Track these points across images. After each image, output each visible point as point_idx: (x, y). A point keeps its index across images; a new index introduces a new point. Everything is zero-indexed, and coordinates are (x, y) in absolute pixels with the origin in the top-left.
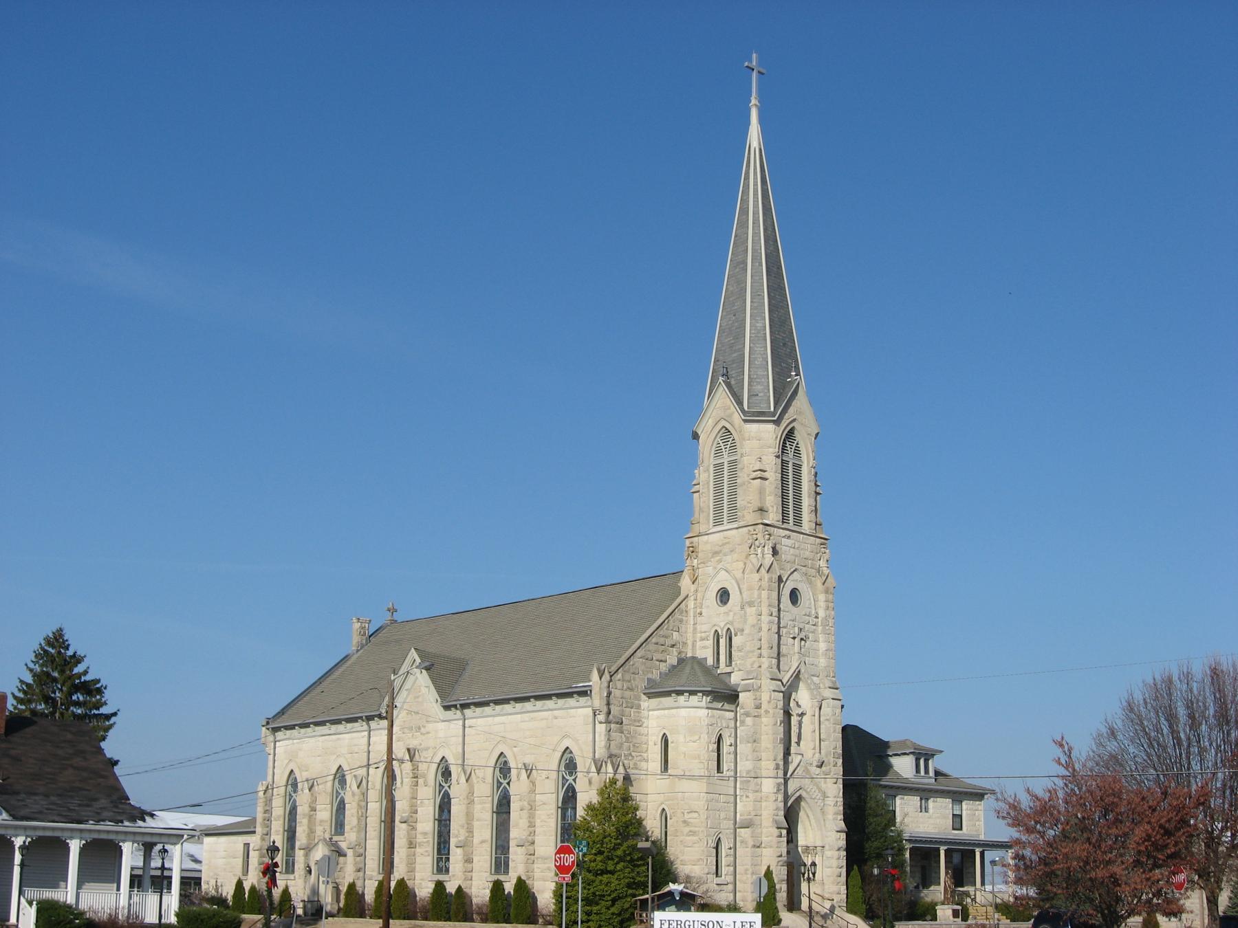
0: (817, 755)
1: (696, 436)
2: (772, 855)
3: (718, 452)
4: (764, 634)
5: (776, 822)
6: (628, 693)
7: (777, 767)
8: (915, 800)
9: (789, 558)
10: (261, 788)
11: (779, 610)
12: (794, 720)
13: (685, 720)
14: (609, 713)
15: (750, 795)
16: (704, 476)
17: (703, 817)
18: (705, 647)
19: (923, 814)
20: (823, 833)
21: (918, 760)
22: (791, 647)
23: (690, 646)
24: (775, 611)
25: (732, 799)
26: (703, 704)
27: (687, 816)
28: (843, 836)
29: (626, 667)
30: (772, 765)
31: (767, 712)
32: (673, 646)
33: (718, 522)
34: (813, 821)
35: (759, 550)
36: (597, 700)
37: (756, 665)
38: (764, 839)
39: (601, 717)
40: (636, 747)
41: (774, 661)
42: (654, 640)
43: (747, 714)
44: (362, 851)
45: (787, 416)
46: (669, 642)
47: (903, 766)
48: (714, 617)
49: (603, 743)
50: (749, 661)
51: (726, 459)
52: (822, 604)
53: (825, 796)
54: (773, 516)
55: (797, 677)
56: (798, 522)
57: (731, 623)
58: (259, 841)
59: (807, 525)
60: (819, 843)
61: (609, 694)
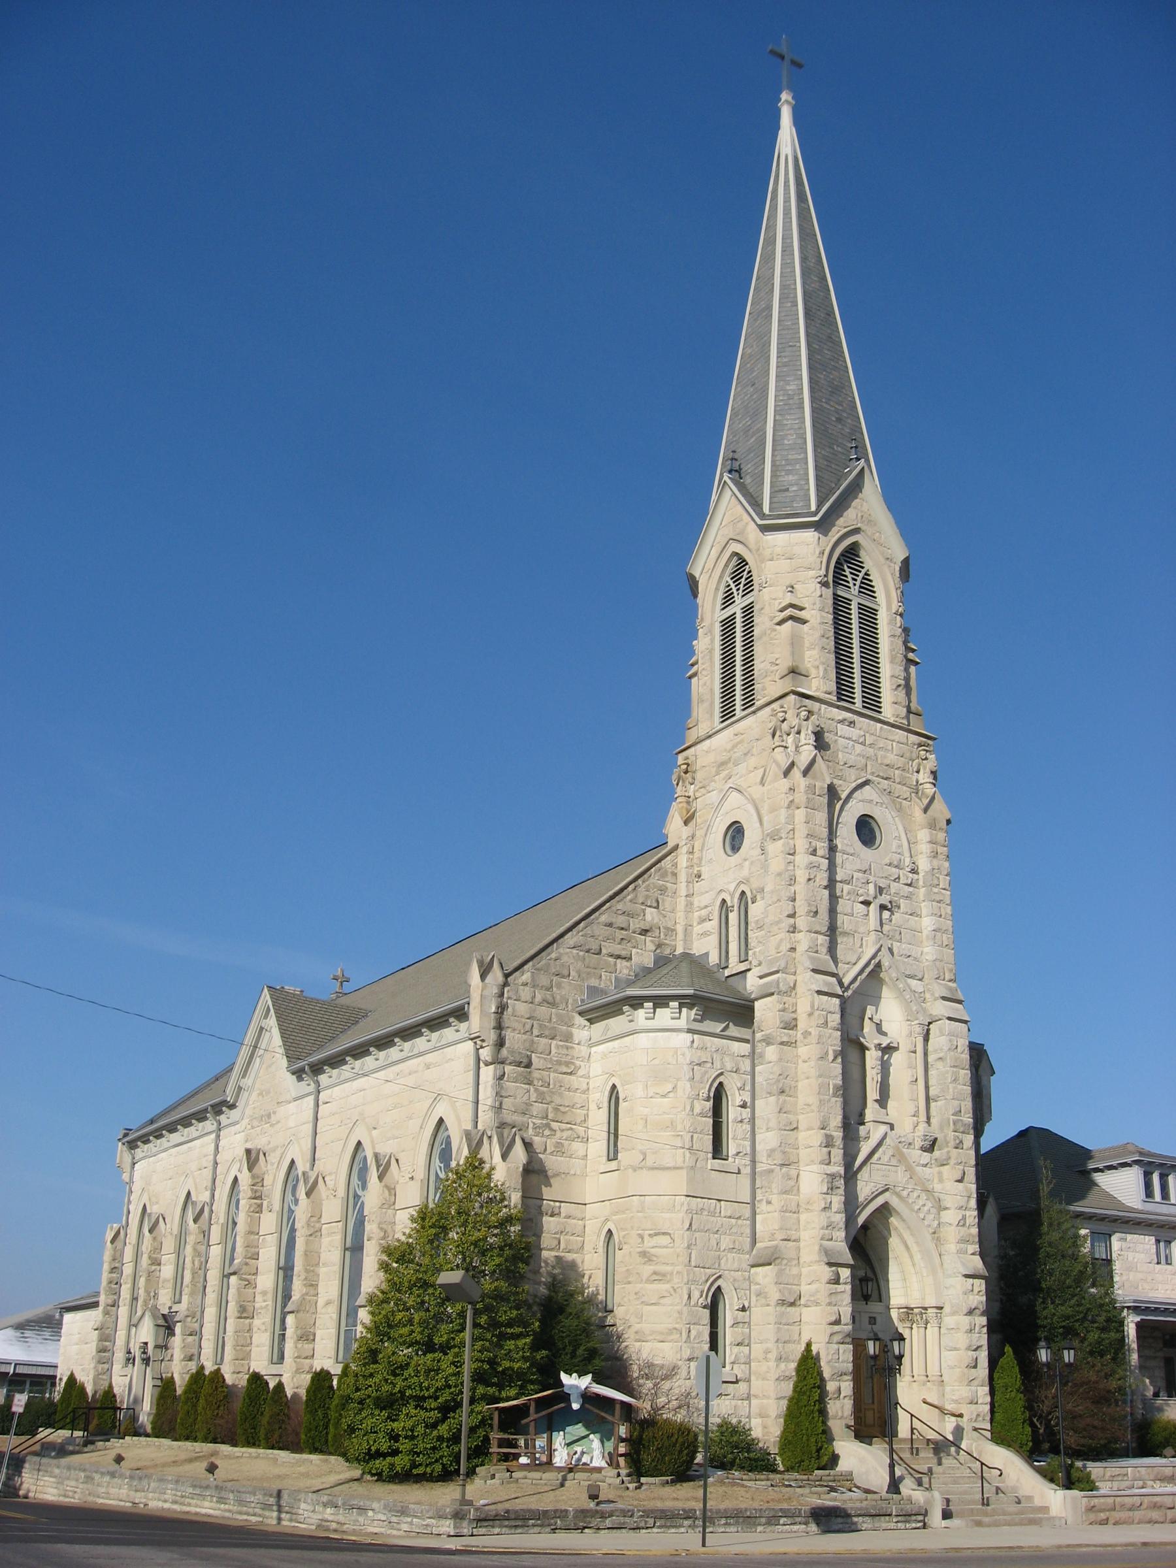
0: (922, 1126)
1: (693, 584)
2: (823, 1320)
3: (728, 599)
4: (800, 888)
5: (826, 1252)
6: (543, 1011)
7: (829, 1143)
8: (1147, 1242)
9: (852, 759)
10: (109, 1236)
11: (832, 849)
12: (872, 1058)
13: (647, 1059)
14: (500, 1043)
15: (774, 1198)
16: (707, 645)
17: (681, 1246)
18: (705, 934)
19: (1163, 1267)
20: (940, 1279)
21: (1147, 1175)
22: (851, 913)
23: (680, 936)
24: (822, 847)
25: (746, 1211)
26: (682, 1023)
27: (649, 1243)
28: (980, 1285)
29: (543, 961)
30: (817, 1138)
31: (806, 1034)
32: (644, 932)
33: (727, 713)
34: (917, 1257)
35: (790, 739)
36: (477, 1021)
37: (785, 947)
38: (804, 1288)
39: (486, 1054)
40: (559, 1115)
41: (822, 940)
42: (603, 918)
43: (768, 1041)
44: (196, 1326)
45: (841, 522)
46: (635, 924)
47: (1122, 1187)
48: (722, 874)
49: (489, 1102)
50: (773, 941)
51: (737, 609)
52: (924, 848)
53: (940, 1208)
54: (820, 682)
55: (874, 974)
56: (872, 701)
57: (745, 881)
58: (101, 1316)
59: (890, 702)
60: (931, 1301)
61: (502, 1009)
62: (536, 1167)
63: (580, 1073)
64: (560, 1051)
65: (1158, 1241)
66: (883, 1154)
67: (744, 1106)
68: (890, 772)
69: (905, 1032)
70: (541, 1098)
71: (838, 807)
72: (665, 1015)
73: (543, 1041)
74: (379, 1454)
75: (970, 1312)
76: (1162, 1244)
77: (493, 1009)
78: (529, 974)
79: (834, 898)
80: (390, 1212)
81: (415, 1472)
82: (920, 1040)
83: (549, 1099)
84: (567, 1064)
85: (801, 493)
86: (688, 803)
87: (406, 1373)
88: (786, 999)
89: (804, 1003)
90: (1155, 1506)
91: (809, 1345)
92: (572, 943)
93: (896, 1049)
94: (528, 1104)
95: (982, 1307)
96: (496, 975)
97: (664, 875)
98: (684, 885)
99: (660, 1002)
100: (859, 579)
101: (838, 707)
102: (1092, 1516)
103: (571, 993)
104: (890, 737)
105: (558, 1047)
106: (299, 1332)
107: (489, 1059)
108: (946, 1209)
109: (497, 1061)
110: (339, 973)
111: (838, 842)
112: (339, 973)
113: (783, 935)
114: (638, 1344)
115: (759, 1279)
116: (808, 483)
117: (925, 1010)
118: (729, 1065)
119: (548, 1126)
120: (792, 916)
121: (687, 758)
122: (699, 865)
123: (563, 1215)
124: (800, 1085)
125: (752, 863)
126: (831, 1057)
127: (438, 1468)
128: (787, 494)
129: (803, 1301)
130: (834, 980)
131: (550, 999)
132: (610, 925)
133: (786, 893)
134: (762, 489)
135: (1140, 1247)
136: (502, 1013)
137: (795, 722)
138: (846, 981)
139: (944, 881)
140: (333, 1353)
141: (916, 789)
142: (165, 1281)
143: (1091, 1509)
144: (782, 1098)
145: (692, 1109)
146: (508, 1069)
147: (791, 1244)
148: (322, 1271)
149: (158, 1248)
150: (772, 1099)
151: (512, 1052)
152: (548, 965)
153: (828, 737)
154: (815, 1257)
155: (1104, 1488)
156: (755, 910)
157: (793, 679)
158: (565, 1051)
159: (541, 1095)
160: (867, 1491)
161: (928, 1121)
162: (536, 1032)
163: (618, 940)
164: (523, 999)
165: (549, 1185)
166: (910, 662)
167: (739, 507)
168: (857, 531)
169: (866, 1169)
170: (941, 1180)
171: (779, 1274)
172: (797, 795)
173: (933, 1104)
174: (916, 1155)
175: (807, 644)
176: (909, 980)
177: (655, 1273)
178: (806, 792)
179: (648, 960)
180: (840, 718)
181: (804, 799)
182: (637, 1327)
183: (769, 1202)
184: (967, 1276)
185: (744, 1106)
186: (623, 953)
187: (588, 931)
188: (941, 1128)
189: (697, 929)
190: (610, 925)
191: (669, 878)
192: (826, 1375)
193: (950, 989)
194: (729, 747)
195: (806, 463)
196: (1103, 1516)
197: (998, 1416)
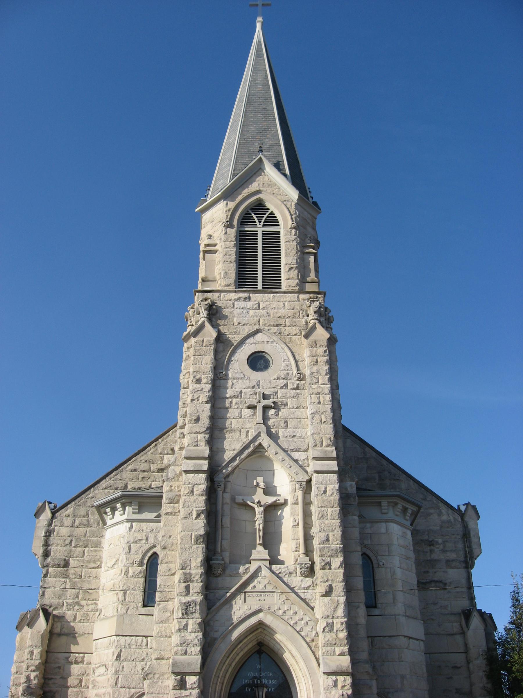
42: (130, 467)
46: (154, 467)
62: (66, 631)
64: (91, 554)
68: (282, 321)
77: (43, 534)
78: (72, 509)
83: (79, 586)
92: (104, 486)
104: (282, 300)
119: (78, 603)
123: (85, 662)
132: (135, 470)
136: (50, 536)
145: (127, 572)
158: (94, 553)
162: (73, 544)
163: (140, 479)
164: (66, 525)
165: (77, 643)
180: (236, 297)
187: (118, 477)
190: (135, 470)
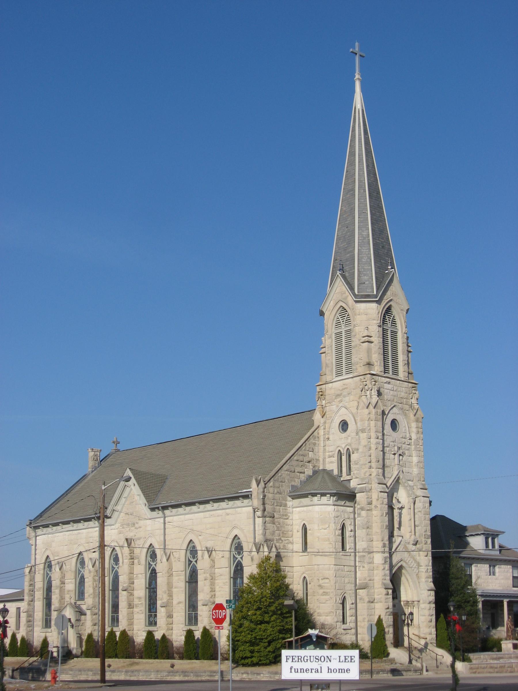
0: (413, 537)
1: (322, 314)
2: (382, 609)
4: (373, 451)
8: (486, 567)
9: (389, 397)
11: (383, 435)
12: (396, 512)
13: (318, 514)
14: (264, 510)
15: (366, 566)
16: (329, 341)
17: (333, 582)
19: (492, 576)
20: (419, 591)
22: (392, 460)
24: (380, 435)
25: (353, 569)
26: (331, 502)
27: (321, 582)
28: (433, 593)
29: (276, 477)
30: (380, 544)
31: (376, 507)
32: (309, 462)
33: (339, 373)
34: (411, 583)
35: (368, 392)
37: (367, 474)
38: (376, 597)
40: (285, 534)
41: (381, 471)
43: (362, 509)
46: (306, 459)
47: (476, 543)
48: (338, 441)
49: (261, 532)
50: (363, 471)
52: (414, 430)
53: (419, 565)
54: (378, 369)
56: (396, 371)
57: (350, 445)
59: (402, 374)
60: (415, 599)
61: (264, 496)
63: (290, 518)
65: (490, 566)
66: (401, 548)
67: (351, 531)
69: (407, 501)
70: (278, 529)
71: (385, 417)
72: (324, 499)
73: (278, 507)
74: (246, 658)
75: (430, 603)
76: (491, 567)
77: (262, 497)
79: (384, 453)
80: (213, 569)
81: (260, 663)
82: (412, 504)
84: (286, 515)
85: (370, 285)
86: (322, 408)
87: (256, 631)
88: (369, 493)
89: (375, 495)
90: (491, 667)
91: (380, 616)
93: (404, 508)
94: (274, 532)
95: (434, 601)
96: (262, 484)
97: (315, 438)
98: (322, 442)
99: (323, 495)
100: (391, 320)
101: (384, 377)
102: (471, 671)
103: (286, 488)
105: (283, 509)
106: (167, 614)
107: (260, 516)
108: (421, 566)
109: (264, 516)
110: (115, 440)
111: (385, 432)
112: (115, 440)
113: (367, 469)
114: (318, 617)
115: (361, 594)
116: (373, 281)
117: (413, 492)
118: (346, 517)
119: (280, 539)
120: (370, 462)
121: (321, 389)
122: (328, 434)
124: (373, 525)
125: (352, 438)
126: (385, 515)
127: (268, 661)
128: (364, 285)
129: (375, 601)
130: (385, 486)
131: (279, 491)
132: (298, 460)
133: (368, 454)
134: (354, 281)
135: (483, 569)
137: (370, 386)
138: (388, 485)
139: (421, 443)
140: (184, 622)
141: (411, 406)
142: (69, 591)
143: (471, 668)
144: (368, 530)
146: (267, 519)
147: (371, 581)
148: (174, 590)
149: (63, 577)
150: (364, 530)
151: (268, 513)
152: (278, 479)
153: (382, 390)
154: (380, 586)
155: (474, 662)
156: (354, 457)
157: (369, 367)
159: (278, 528)
160: (401, 664)
161: (415, 535)
162: (275, 504)
165: (282, 561)
166: (409, 352)
167: (344, 287)
168: (391, 300)
169: (395, 553)
170: (419, 556)
171: (368, 592)
172: (371, 416)
173: (416, 528)
174: (411, 547)
175: (373, 352)
176: (409, 482)
177: (324, 592)
178: (375, 415)
179: (311, 473)
181: (374, 417)
182: (318, 611)
183: (363, 567)
184: (429, 590)
185: (351, 531)
186: (302, 471)
187: (291, 464)
188: (420, 537)
189: (328, 460)
190: (298, 460)
191: (317, 439)
192: (385, 626)
193: (423, 485)
194: (341, 388)
195: (372, 271)
196: (474, 671)
197: (438, 639)
